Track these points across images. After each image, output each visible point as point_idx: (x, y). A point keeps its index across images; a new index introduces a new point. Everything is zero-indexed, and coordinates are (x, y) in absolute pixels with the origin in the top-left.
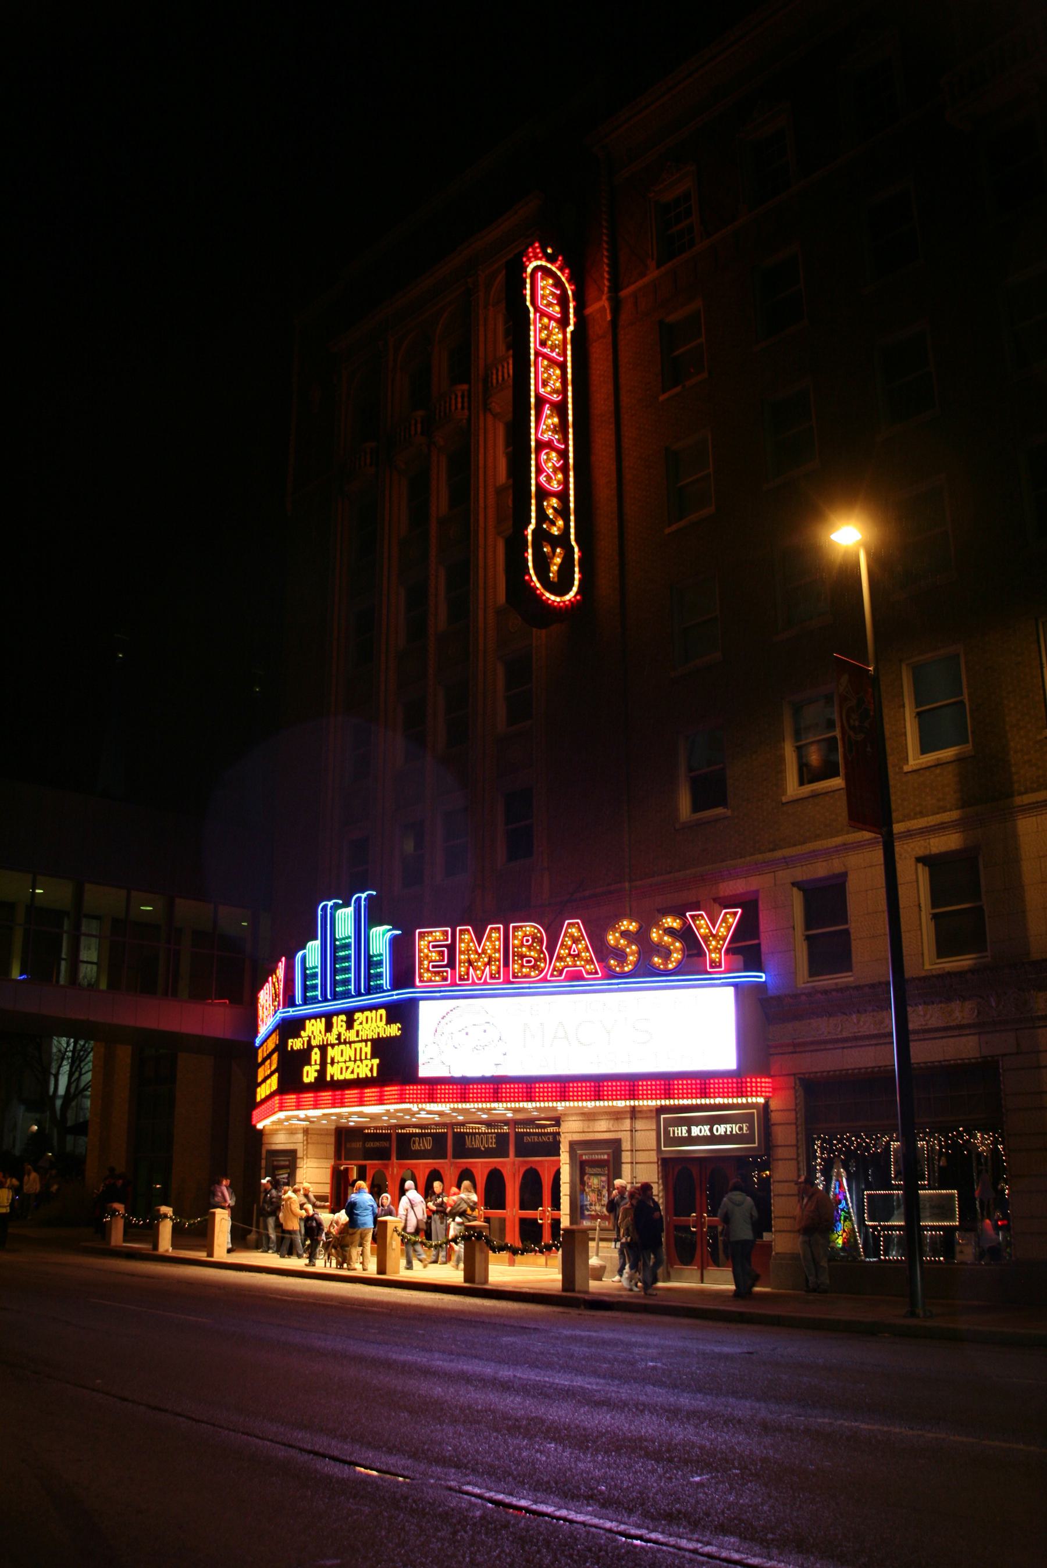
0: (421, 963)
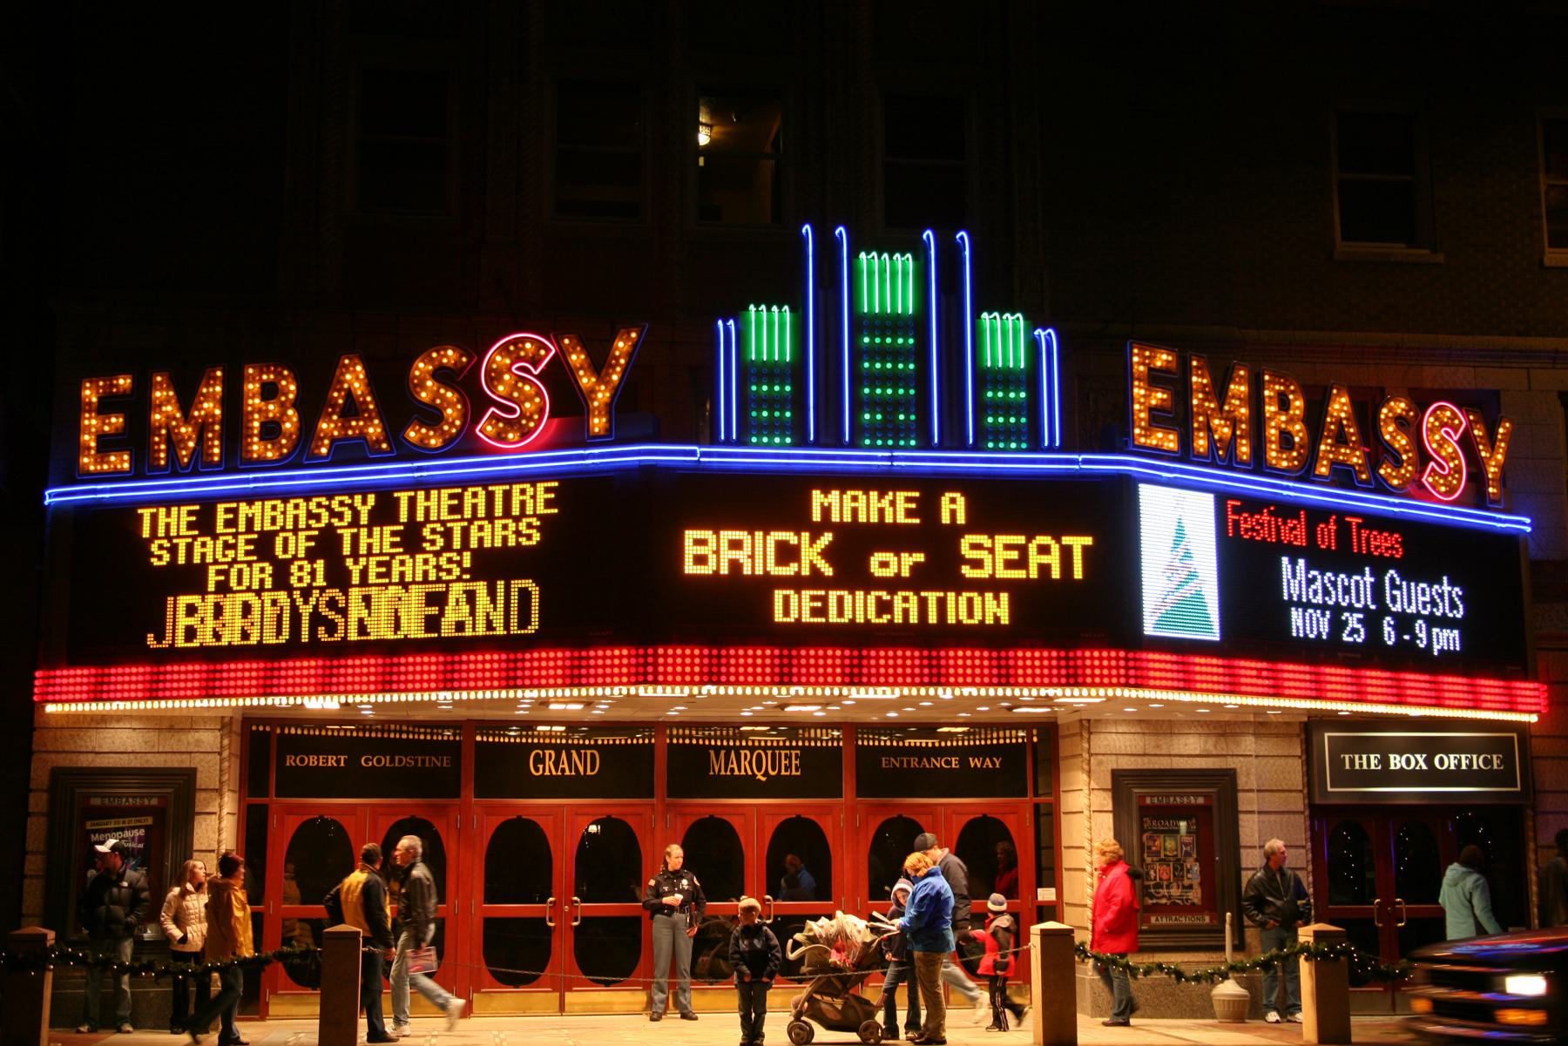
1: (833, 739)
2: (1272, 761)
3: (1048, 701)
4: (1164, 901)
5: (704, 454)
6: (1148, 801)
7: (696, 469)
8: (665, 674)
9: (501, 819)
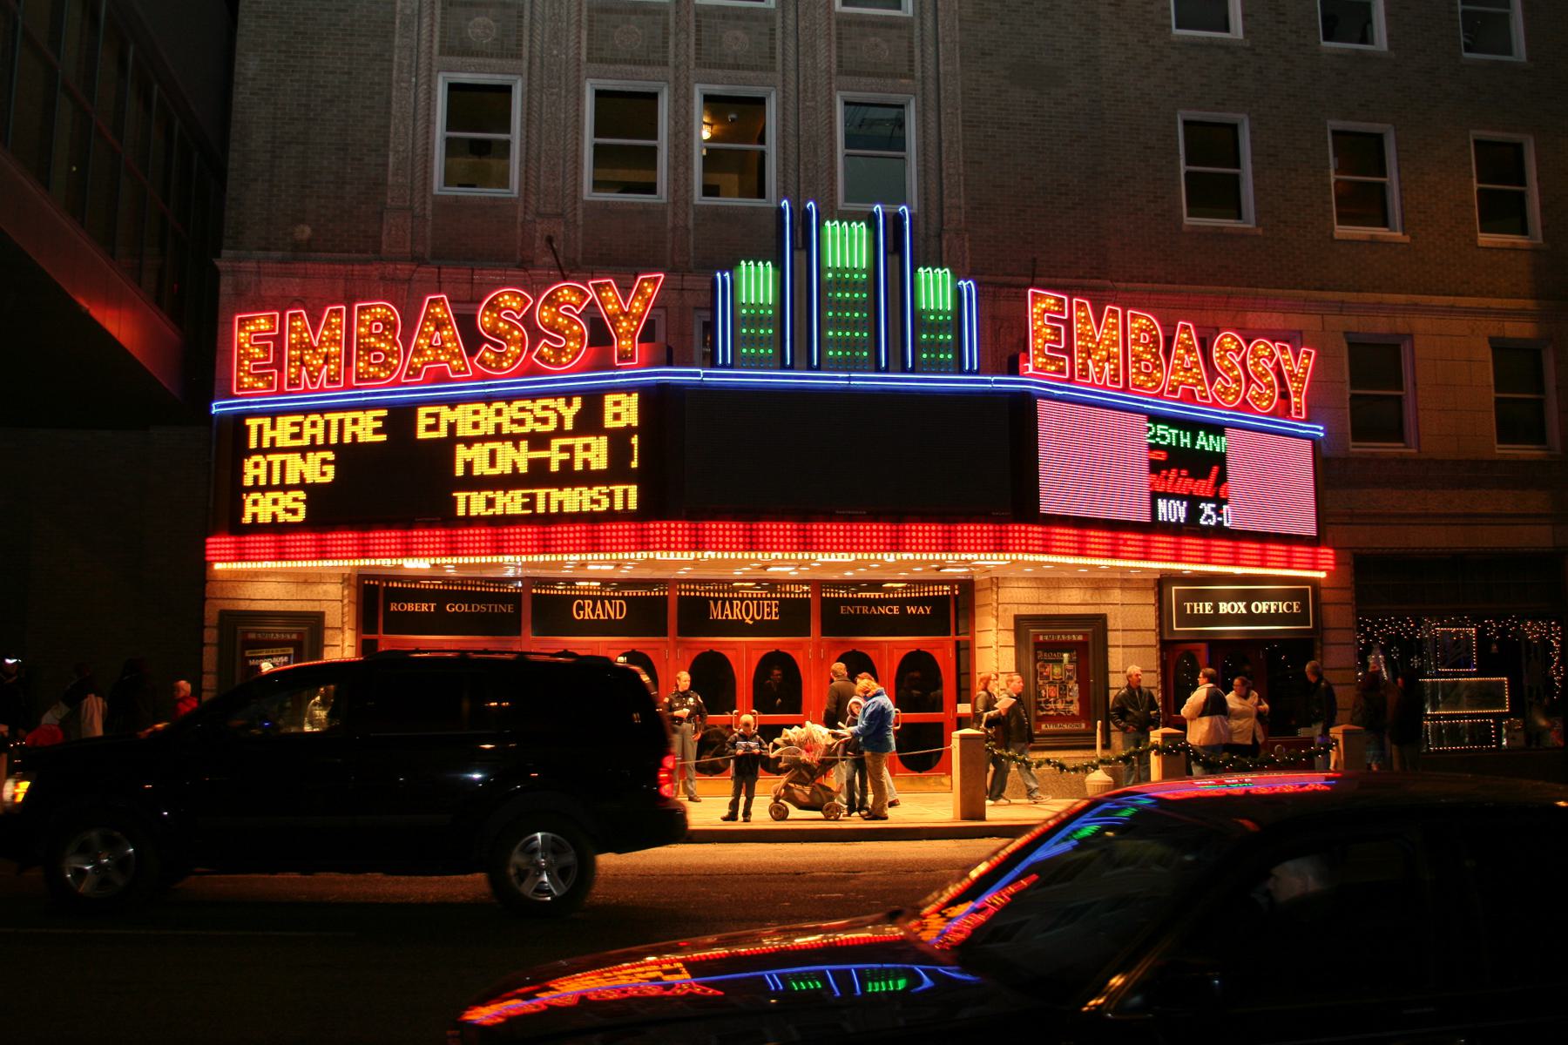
0: (240, 363)
5: (706, 375)
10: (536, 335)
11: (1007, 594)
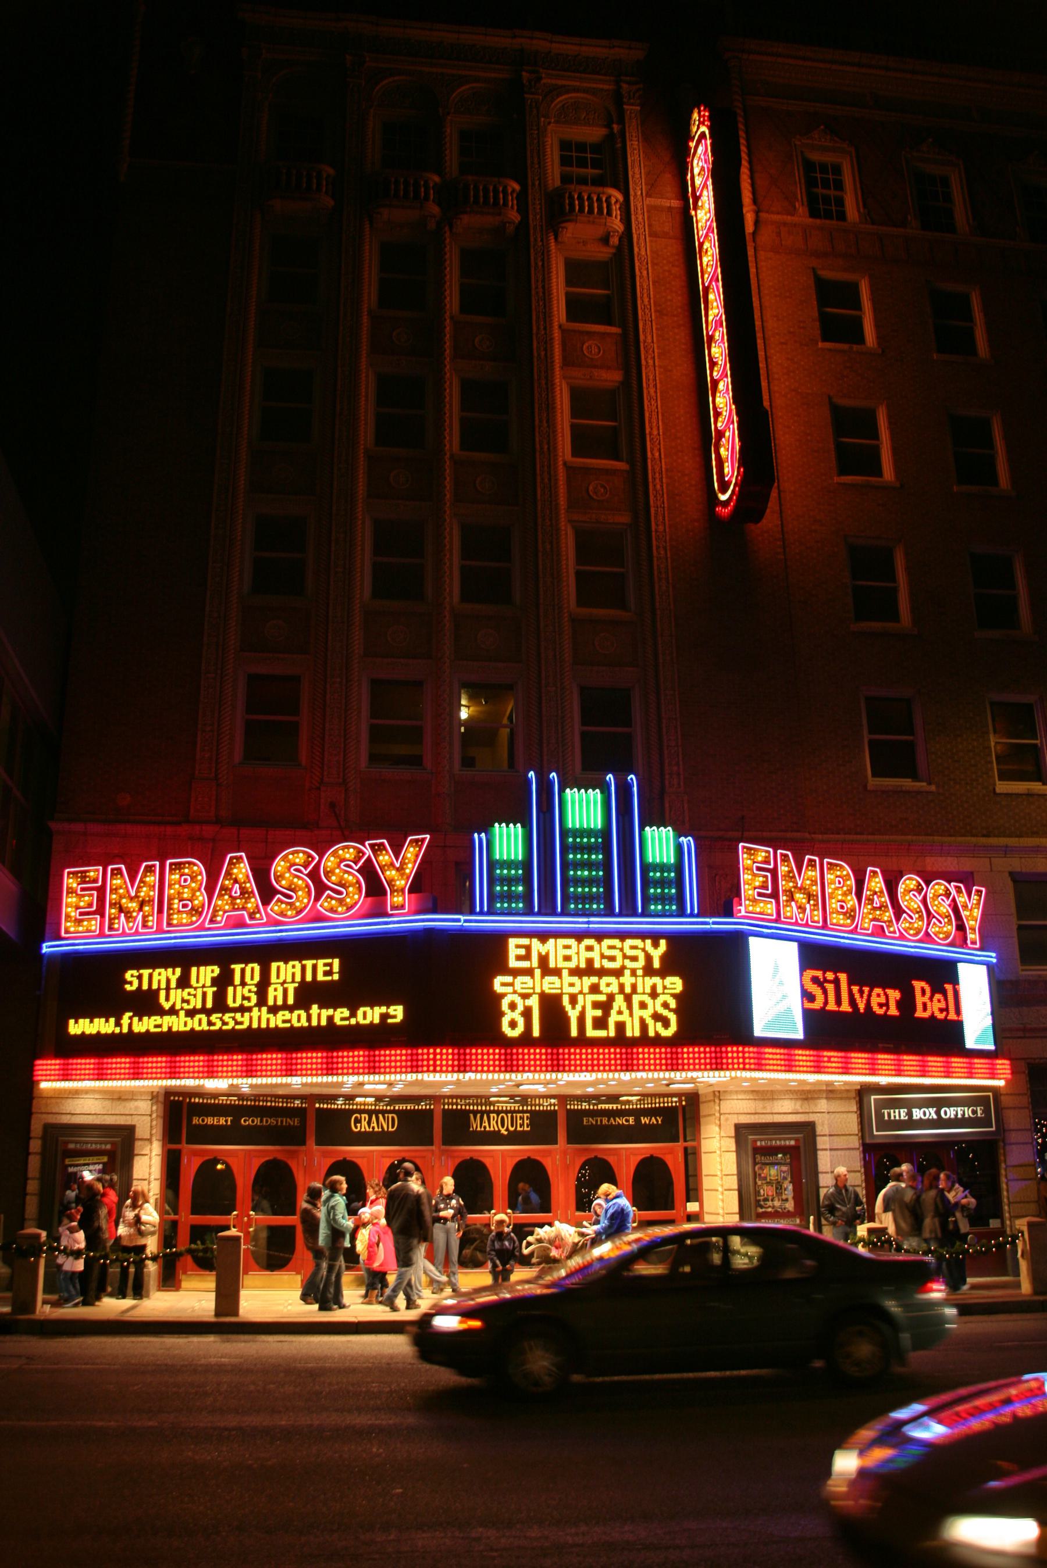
1: (550, 1105)
2: (838, 1115)
3: (693, 1081)
4: (770, 1210)
5: (466, 921)
6: (759, 1144)
7: (461, 930)
8: (441, 1066)
9: (333, 1160)
10: (321, 888)
11: (727, 1106)
